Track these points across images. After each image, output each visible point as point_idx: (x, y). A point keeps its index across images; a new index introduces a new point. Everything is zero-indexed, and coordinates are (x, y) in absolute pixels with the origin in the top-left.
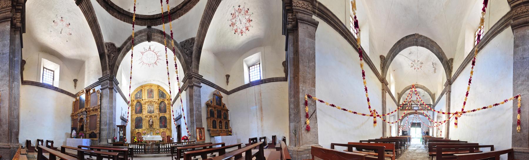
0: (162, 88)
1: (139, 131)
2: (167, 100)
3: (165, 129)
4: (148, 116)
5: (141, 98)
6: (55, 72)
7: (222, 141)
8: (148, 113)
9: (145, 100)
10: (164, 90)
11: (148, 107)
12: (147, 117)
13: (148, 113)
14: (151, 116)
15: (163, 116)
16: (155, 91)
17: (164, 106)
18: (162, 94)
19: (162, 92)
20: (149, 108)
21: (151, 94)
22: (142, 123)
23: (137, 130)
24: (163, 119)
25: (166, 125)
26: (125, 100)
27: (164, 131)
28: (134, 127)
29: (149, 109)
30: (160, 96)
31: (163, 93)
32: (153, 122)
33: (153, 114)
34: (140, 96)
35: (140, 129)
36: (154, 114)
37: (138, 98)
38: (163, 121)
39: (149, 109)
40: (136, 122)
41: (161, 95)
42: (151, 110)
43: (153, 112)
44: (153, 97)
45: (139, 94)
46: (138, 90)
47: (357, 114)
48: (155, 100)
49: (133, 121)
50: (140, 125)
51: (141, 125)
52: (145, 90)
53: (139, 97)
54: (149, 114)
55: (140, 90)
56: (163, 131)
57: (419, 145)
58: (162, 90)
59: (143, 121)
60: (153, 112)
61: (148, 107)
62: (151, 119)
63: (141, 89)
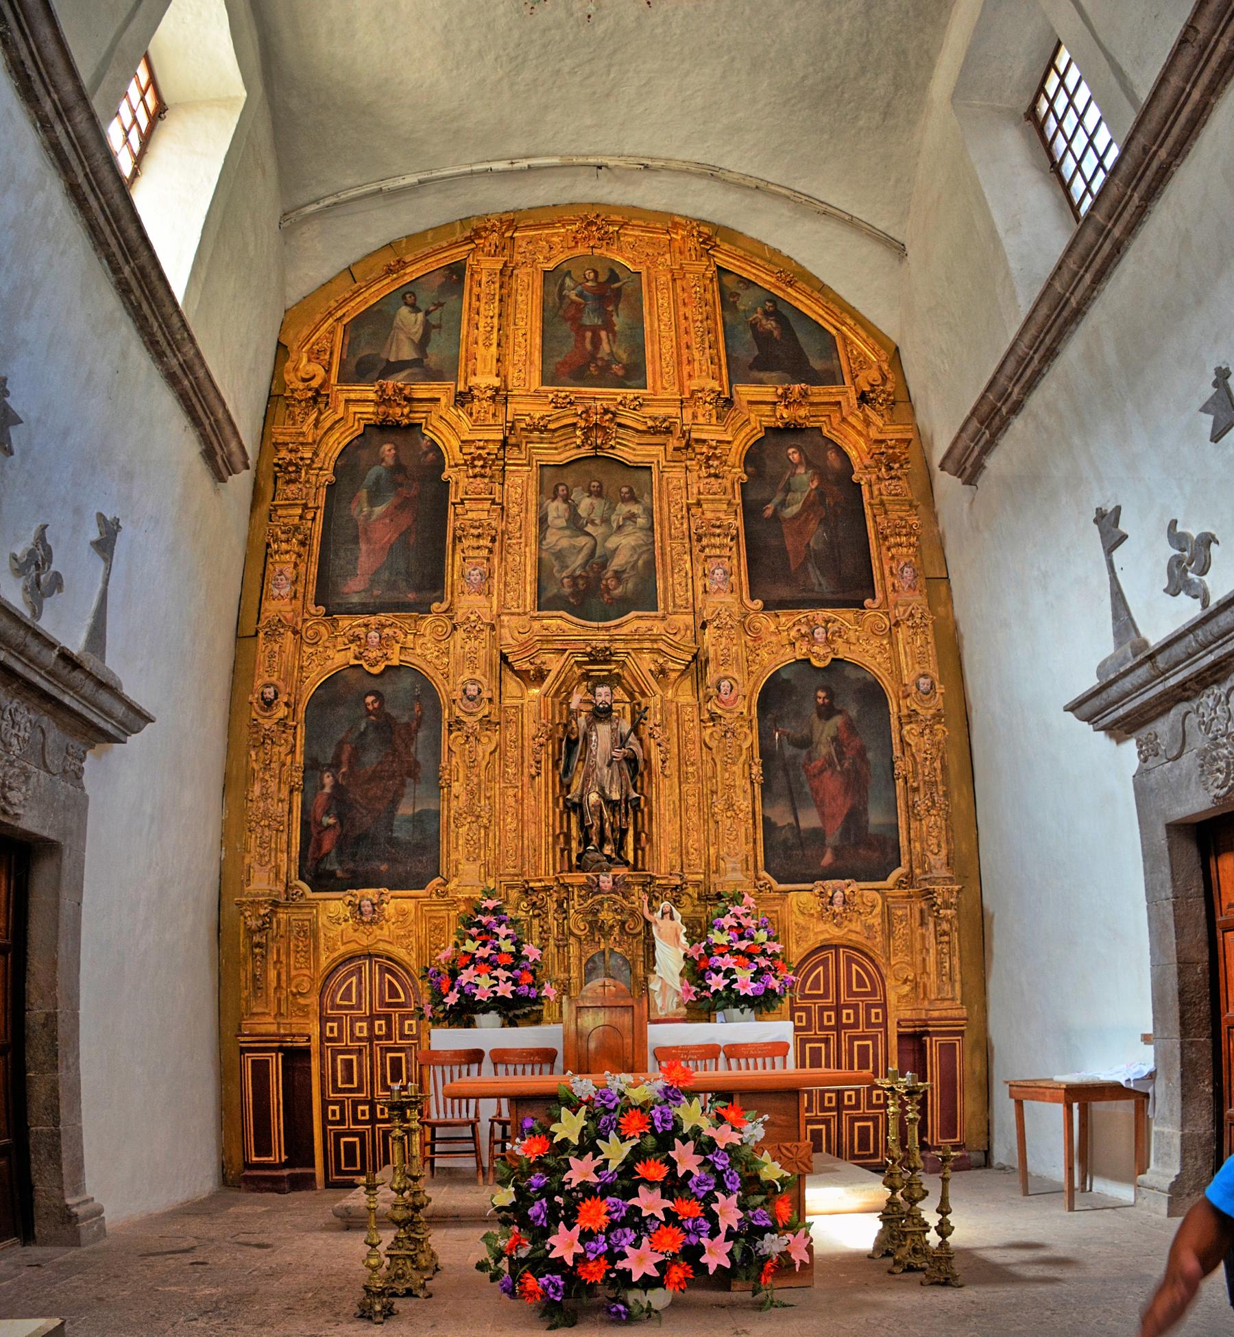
0: (758, 251)
1: (384, 938)
2: (863, 398)
3: (866, 892)
4: (554, 664)
5: (435, 375)
6: (1024, 107)
7: (1058, 1102)
8: (544, 602)
9: (500, 396)
10: (796, 275)
11: (556, 509)
12: (540, 676)
13: (544, 602)
14: (600, 656)
15: (821, 657)
16: (663, 299)
17: (821, 493)
18: (770, 324)
19: (774, 299)
20: (575, 523)
21: (609, 326)
22: (437, 785)
23: (335, 905)
24: (827, 712)
25: (875, 818)
26: (190, 411)
27: (852, 931)
28: (288, 862)
29: (558, 538)
30: (748, 351)
31: (777, 309)
32: (635, 767)
33: (633, 622)
34: (422, 344)
35: (397, 903)
36: (658, 628)
37: (401, 366)
38: (824, 750)
39: (558, 538)
40: (312, 767)
41: (761, 338)
42: (598, 562)
43: (645, 599)
44: (634, 374)
45: (409, 321)
46: (412, 272)
47: (1174, 523)
48: (673, 411)
49: (263, 741)
50: (405, 809)
51: (418, 820)
52: (506, 273)
53: (408, 353)
54: (560, 623)
55: (433, 263)
56: (826, 931)
57: (263, 895)
58: (766, 280)
59: (448, 740)
60: (645, 599)
61: (556, 509)
62: (602, 714)
63: (458, 254)
